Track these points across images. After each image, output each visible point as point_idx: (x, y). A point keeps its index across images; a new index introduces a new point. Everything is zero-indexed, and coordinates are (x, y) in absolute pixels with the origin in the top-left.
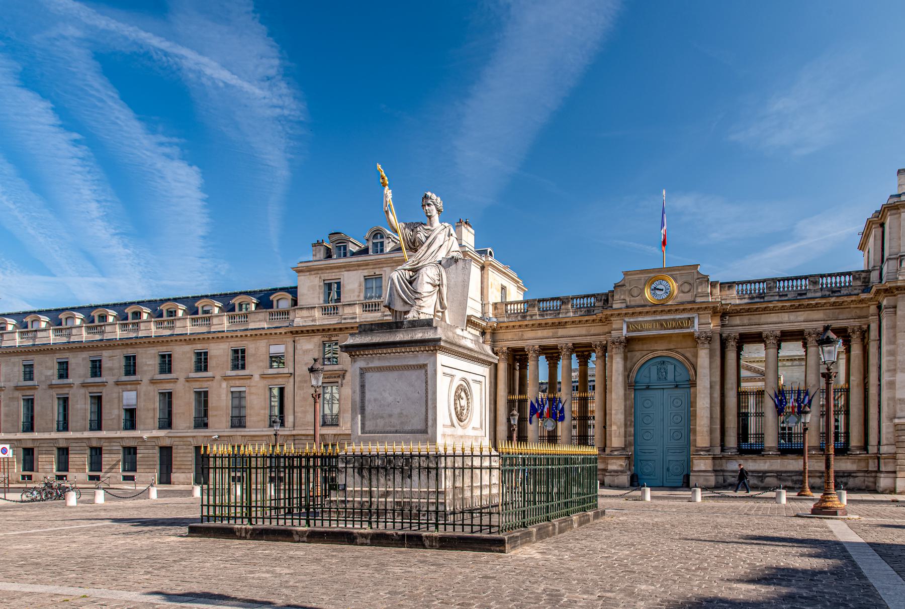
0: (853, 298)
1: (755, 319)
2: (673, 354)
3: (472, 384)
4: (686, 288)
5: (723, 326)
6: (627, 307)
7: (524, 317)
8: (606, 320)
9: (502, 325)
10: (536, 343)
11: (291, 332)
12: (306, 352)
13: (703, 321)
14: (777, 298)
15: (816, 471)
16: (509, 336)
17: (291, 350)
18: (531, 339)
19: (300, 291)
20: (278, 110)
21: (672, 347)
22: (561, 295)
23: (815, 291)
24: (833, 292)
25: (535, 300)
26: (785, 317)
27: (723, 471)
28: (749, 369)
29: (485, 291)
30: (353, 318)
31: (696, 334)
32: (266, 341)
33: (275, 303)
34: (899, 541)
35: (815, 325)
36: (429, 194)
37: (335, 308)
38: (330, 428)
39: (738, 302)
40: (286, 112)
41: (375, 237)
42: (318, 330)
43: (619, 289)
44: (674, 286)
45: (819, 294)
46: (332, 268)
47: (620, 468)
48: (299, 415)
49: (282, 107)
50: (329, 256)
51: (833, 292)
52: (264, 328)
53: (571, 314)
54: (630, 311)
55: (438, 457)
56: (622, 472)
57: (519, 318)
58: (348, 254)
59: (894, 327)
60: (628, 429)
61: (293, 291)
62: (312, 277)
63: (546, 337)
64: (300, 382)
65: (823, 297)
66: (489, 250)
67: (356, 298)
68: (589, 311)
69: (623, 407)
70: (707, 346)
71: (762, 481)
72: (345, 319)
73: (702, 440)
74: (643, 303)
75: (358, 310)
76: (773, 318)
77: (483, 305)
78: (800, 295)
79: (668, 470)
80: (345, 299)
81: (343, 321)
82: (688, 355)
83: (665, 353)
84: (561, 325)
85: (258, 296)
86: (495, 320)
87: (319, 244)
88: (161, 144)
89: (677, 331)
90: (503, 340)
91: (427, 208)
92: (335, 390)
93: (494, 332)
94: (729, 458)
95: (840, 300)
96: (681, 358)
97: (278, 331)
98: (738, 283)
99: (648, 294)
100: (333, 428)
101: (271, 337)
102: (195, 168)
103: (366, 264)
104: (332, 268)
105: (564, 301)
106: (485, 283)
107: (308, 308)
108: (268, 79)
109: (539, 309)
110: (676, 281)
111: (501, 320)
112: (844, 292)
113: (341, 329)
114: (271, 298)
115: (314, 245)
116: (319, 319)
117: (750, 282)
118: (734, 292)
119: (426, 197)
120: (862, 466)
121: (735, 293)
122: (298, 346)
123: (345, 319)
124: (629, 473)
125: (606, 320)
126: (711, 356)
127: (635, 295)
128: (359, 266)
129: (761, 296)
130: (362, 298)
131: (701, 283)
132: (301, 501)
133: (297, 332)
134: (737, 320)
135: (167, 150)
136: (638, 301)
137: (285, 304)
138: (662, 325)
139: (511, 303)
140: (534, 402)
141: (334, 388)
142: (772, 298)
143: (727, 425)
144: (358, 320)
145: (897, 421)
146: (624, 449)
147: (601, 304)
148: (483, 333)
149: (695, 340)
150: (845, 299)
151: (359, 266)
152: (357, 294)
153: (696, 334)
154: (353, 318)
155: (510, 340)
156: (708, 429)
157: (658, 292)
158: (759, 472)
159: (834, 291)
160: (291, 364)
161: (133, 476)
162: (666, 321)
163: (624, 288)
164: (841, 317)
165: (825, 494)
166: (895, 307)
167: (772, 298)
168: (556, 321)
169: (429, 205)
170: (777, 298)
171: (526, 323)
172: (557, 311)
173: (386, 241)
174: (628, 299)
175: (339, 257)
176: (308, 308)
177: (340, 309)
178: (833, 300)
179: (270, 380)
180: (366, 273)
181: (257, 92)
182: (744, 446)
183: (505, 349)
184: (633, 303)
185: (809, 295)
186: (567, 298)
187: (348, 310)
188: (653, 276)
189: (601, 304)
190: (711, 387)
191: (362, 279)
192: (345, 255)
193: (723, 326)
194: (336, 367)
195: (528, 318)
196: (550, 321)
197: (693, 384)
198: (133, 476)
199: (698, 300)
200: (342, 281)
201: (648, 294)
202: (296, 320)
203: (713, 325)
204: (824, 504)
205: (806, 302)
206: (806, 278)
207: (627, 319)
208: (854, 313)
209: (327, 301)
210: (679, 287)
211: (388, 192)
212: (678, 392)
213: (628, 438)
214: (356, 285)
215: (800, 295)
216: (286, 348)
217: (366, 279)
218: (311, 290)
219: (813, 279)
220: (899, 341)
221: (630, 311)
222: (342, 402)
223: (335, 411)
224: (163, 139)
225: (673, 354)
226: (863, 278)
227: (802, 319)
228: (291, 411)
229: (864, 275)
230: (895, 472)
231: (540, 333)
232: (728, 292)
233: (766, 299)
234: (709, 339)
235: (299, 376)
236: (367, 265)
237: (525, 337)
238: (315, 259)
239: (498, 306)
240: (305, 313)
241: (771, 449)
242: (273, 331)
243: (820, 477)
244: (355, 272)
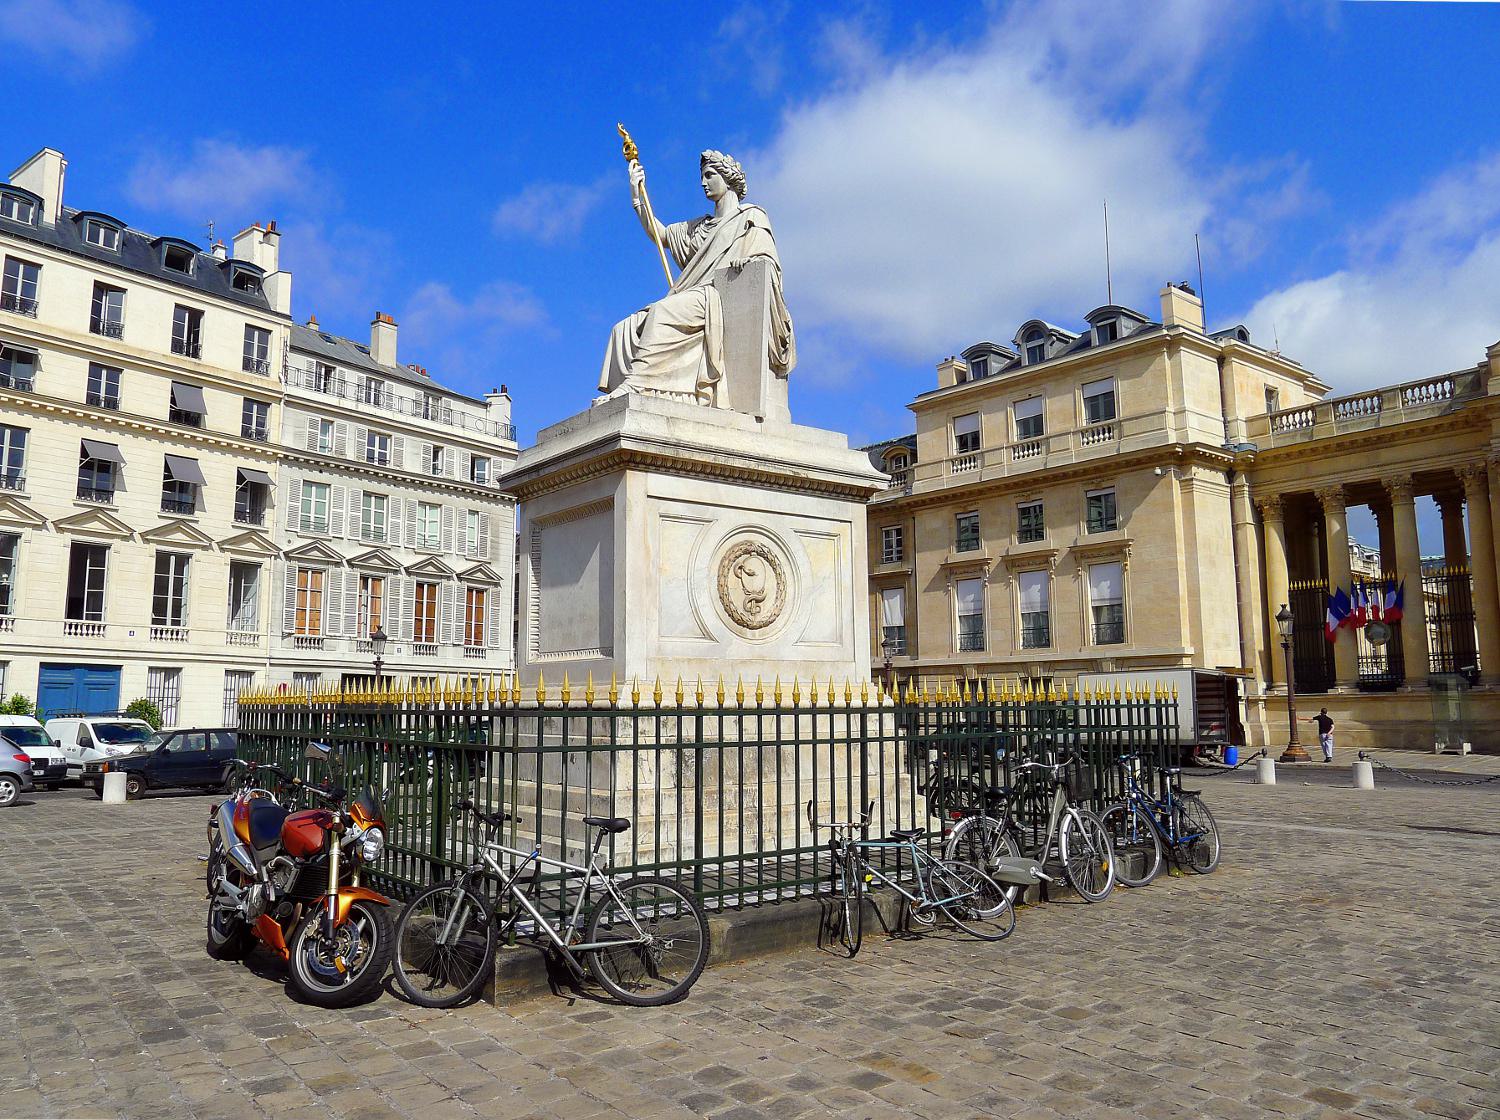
3: (795, 543)
10: (1336, 482)
16: (1280, 473)
18: (1324, 478)
36: (707, 153)
42: (946, 497)
55: (612, 713)
90: (1271, 482)
91: (705, 181)
116: (949, 479)
119: (704, 161)
132: (1148, 734)
139: (1287, 413)
148: (1230, 476)
155: (1290, 481)
169: (708, 175)
182: (23, 788)
211: (636, 173)
231: (1342, 462)
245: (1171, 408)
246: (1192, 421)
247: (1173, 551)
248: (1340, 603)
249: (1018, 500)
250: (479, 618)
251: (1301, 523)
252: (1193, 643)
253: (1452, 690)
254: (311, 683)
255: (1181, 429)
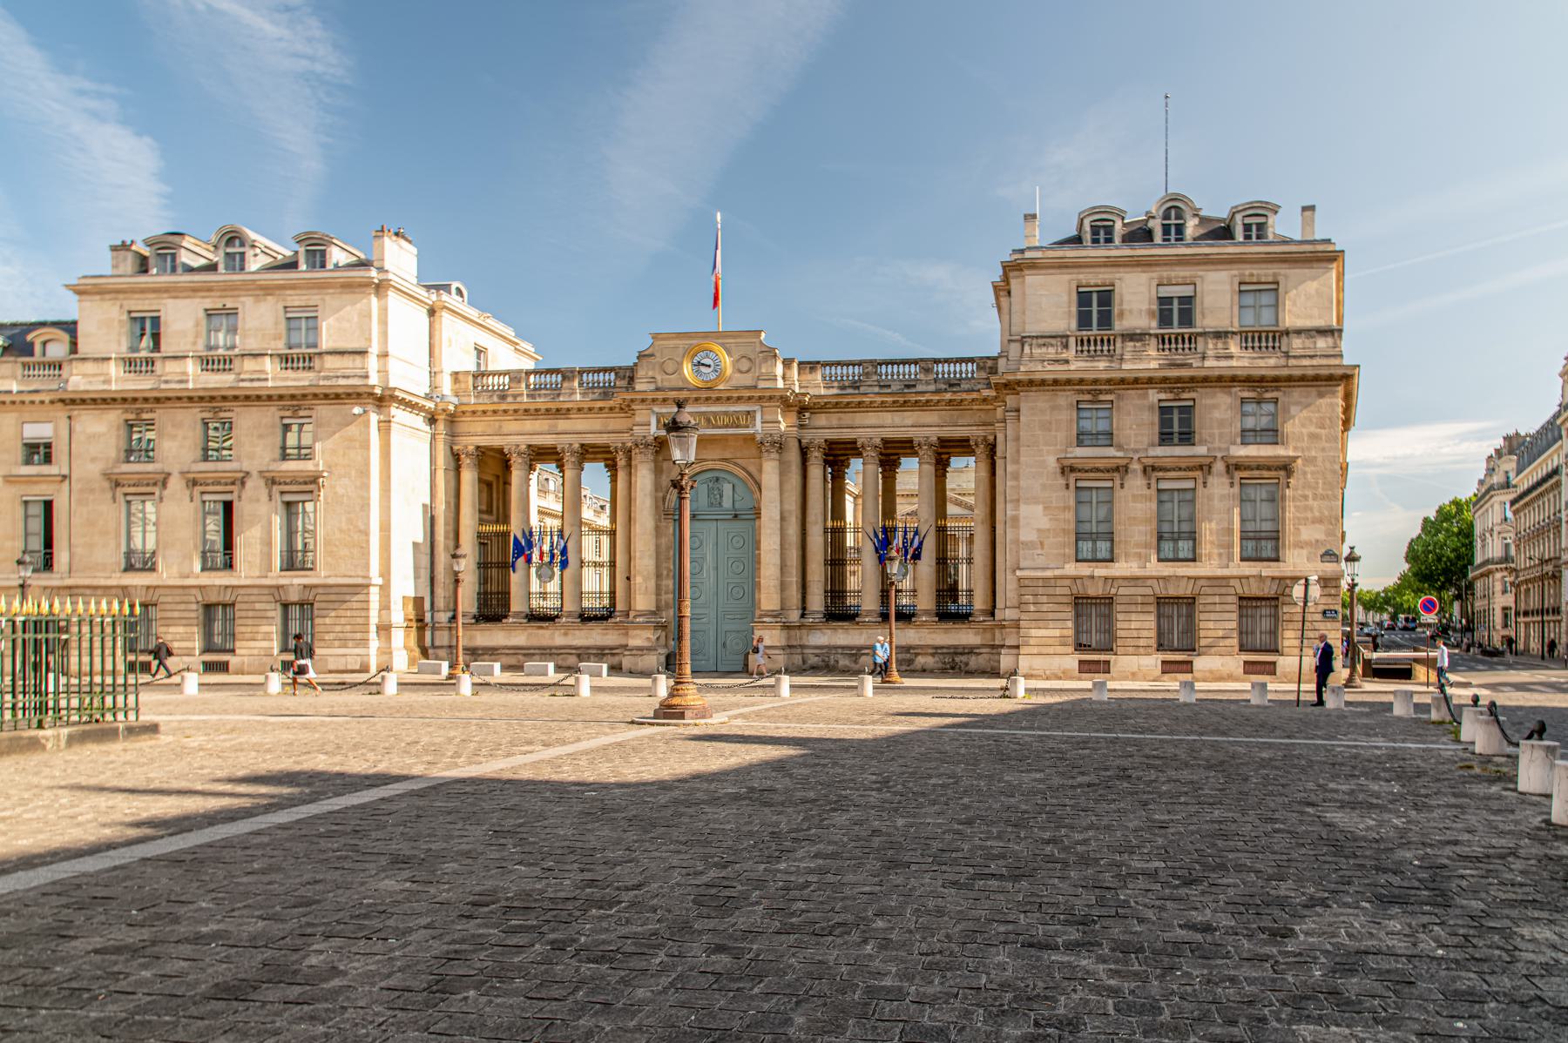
0: (975, 395)
1: (848, 419)
2: (731, 467)
4: (745, 365)
5: (802, 426)
6: (658, 389)
7: (503, 397)
8: (626, 409)
9: (464, 408)
10: (523, 442)
11: (62, 401)
12: (92, 437)
13: (768, 417)
14: (876, 389)
15: (928, 646)
16: (478, 427)
17: (65, 433)
18: (515, 435)
19: (81, 328)
20: (304, 63)
21: (728, 456)
22: (563, 365)
23: (928, 383)
24: (951, 385)
25: (520, 371)
26: (888, 418)
27: (803, 647)
28: (959, 504)
29: (437, 351)
30: (181, 382)
31: (758, 438)
32: (14, 415)
33: (38, 349)
34: (1564, 705)
35: (926, 432)
37: (150, 362)
38: (139, 574)
39: (823, 392)
40: (319, 68)
41: (230, 242)
42: (114, 400)
43: (644, 361)
44: (727, 361)
45: (932, 388)
46: (143, 291)
47: (646, 644)
48: (78, 551)
49: (312, 59)
50: (143, 265)
51: (951, 385)
52: (10, 392)
53: (578, 397)
54: (660, 395)
56: (649, 649)
57: (495, 399)
58: (180, 270)
59: (1017, 439)
60: (664, 582)
61: (70, 328)
62: (107, 305)
63: (539, 432)
64: (81, 491)
65: (938, 392)
66: (455, 285)
67: (189, 347)
68: (606, 393)
69: (653, 548)
70: (775, 455)
71: (856, 662)
72: (166, 382)
73: (769, 599)
74: (681, 385)
75: (191, 367)
76: (871, 418)
77: (433, 374)
78: (908, 386)
79: (724, 645)
80: (167, 347)
81: (163, 386)
82: (752, 469)
83: (719, 465)
84: (560, 413)
85: (9, 333)
86: (455, 400)
87: (124, 247)
88: (82, 93)
89: (731, 431)
92: (150, 507)
93: (452, 419)
94: (811, 628)
95: (958, 397)
96: (742, 474)
97: (37, 398)
98: (825, 364)
99: (687, 369)
100: (145, 574)
101: (25, 408)
102: (147, 140)
103: (208, 289)
104: (143, 291)
105: (567, 375)
106: (437, 338)
107: (96, 359)
108: (288, 9)
109: (528, 386)
110: (729, 354)
111: (465, 400)
112: (964, 386)
113: (157, 400)
114: (29, 337)
115: (114, 249)
116: (116, 379)
117: (838, 363)
118: (818, 376)
120: (987, 639)
121: (819, 377)
122: (78, 427)
123: (166, 382)
124: (664, 651)
125: (626, 409)
126: (783, 473)
127: (670, 370)
128: (195, 290)
129: (855, 385)
130: (201, 346)
131: (765, 360)
133: (73, 401)
134: (821, 420)
135: (94, 104)
136: (673, 381)
137: (57, 350)
138: (708, 420)
139: (494, 374)
140: (520, 537)
141: (149, 505)
142: (870, 390)
143: (810, 577)
144: (191, 386)
145: (1018, 573)
146: (653, 613)
147: (624, 383)
148: (432, 420)
149: (759, 446)
150: (964, 396)
151: (194, 290)
152: (190, 339)
153: (758, 438)
154: (181, 382)
155: (477, 435)
156: (777, 583)
157: (703, 369)
158: (851, 648)
159: (952, 384)
160: (65, 459)
161: (227, 663)
162: (715, 414)
163: (651, 359)
164: (960, 422)
165: (677, 683)
166: (1018, 410)
167: (870, 390)
168: (553, 406)
170: (876, 389)
171: (504, 407)
172: (556, 391)
173: (250, 253)
174: (659, 378)
175: (162, 271)
176: (96, 359)
177: (158, 365)
178: (948, 396)
179: (23, 487)
180: (208, 303)
181: (269, 28)
183: (471, 448)
184: (666, 384)
185: (920, 388)
186: (572, 371)
187: (172, 367)
188: (695, 344)
189: (624, 383)
190: (783, 519)
191: (202, 314)
192: (174, 269)
193: (802, 426)
194: (150, 467)
195: (510, 399)
196: (543, 407)
197: (757, 513)
198: (227, 663)
199: (762, 385)
200: (162, 314)
201: (687, 369)
202: (73, 379)
203: (784, 423)
204: (675, 701)
205: (913, 398)
206: (916, 362)
207: (656, 409)
208: (976, 418)
209: (134, 349)
210: (734, 363)
212: (737, 525)
213: (664, 597)
214: (190, 324)
215: (908, 386)
216: (56, 430)
217: (209, 314)
218: (104, 330)
219: (927, 365)
220: (1022, 459)
221: (660, 395)
222: (162, 529)
223: (150, 546)
224: (87, 85)
225: (731, 467)
226: (988, 365)
227: (909, 422)
228: (65, 544)
229: (990, 363)
230: (1018, 647)
231: (529, 425)
232: (810, 377)
233: (862, 390)
234: (780, 446)
235: (79, 480)
236: (210, 290)
237: (505, 430)
238: (116, 272)
239: (461, 377)
240: (90, 367)
241: (869, 613)
242: (27, 398)
243: (933, 655)
244: (187, 301)
245: (374, 350)
246: (393, 365)
247: (366, 486)
248: (523, 549)
249: (1163, 396)
250: (1098, 470)
251: (495, 471)
252: (381, 575)
253: (1137, 650)
254: (193, 615)
255: (383, 372)
